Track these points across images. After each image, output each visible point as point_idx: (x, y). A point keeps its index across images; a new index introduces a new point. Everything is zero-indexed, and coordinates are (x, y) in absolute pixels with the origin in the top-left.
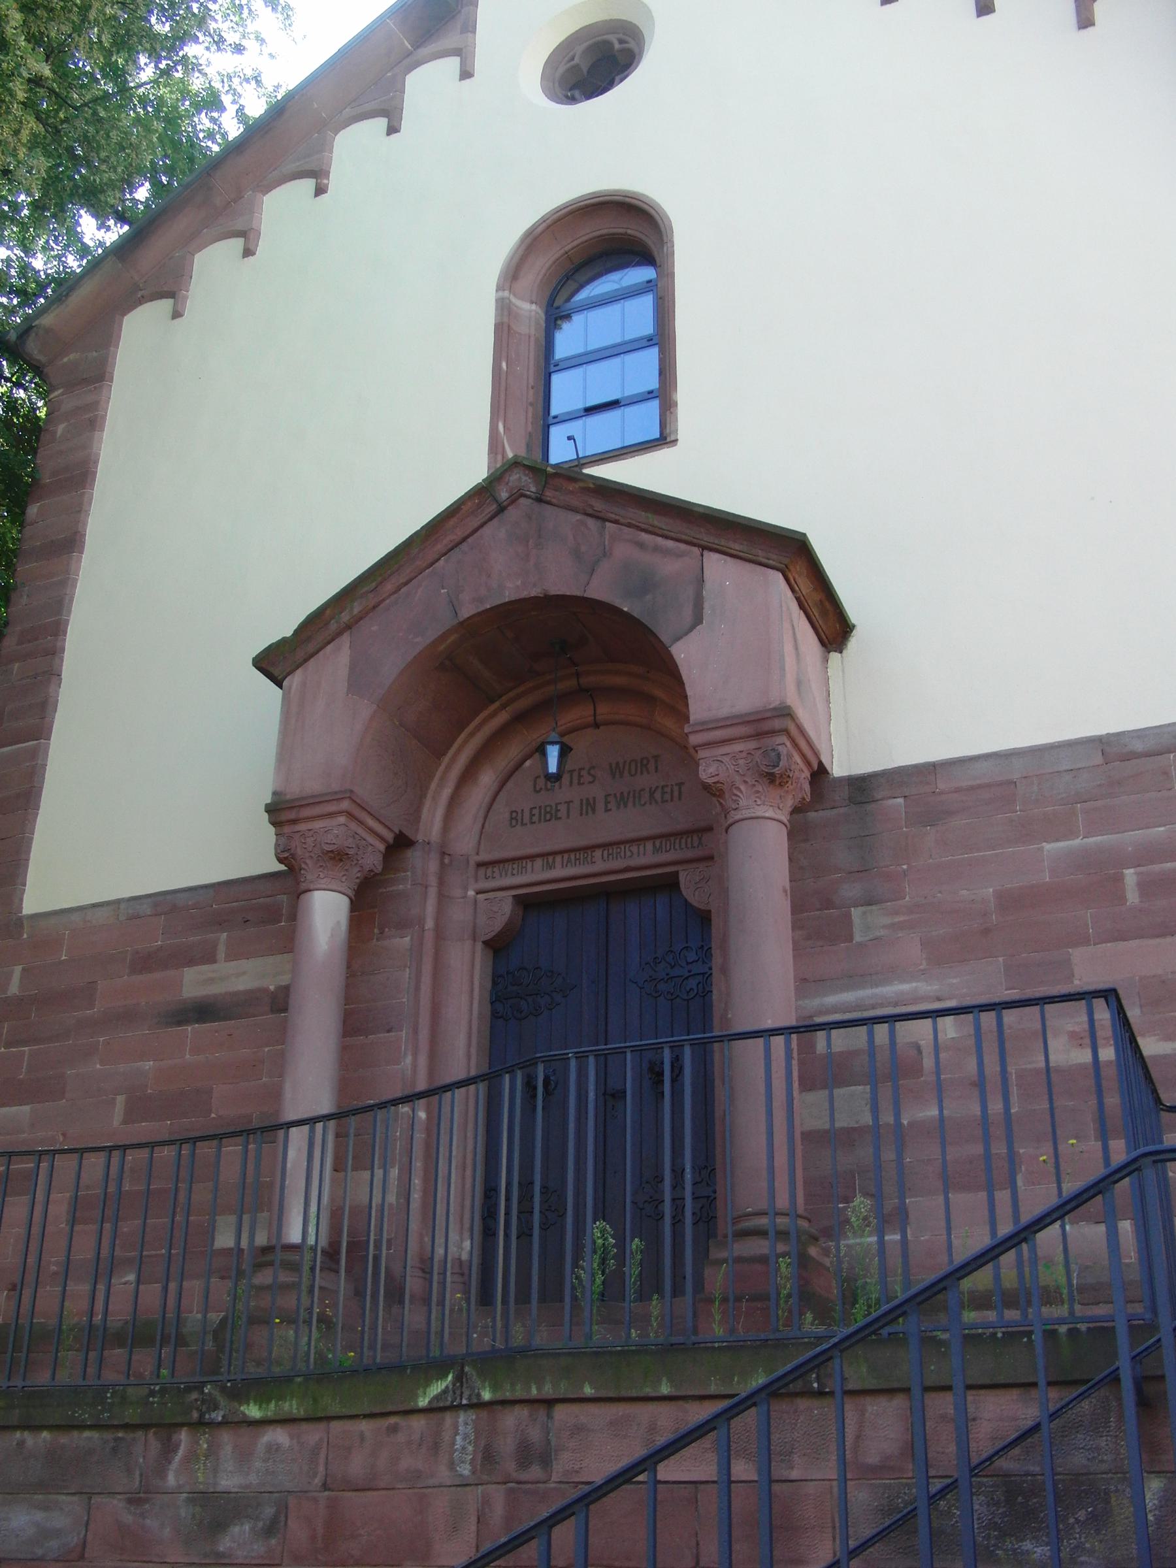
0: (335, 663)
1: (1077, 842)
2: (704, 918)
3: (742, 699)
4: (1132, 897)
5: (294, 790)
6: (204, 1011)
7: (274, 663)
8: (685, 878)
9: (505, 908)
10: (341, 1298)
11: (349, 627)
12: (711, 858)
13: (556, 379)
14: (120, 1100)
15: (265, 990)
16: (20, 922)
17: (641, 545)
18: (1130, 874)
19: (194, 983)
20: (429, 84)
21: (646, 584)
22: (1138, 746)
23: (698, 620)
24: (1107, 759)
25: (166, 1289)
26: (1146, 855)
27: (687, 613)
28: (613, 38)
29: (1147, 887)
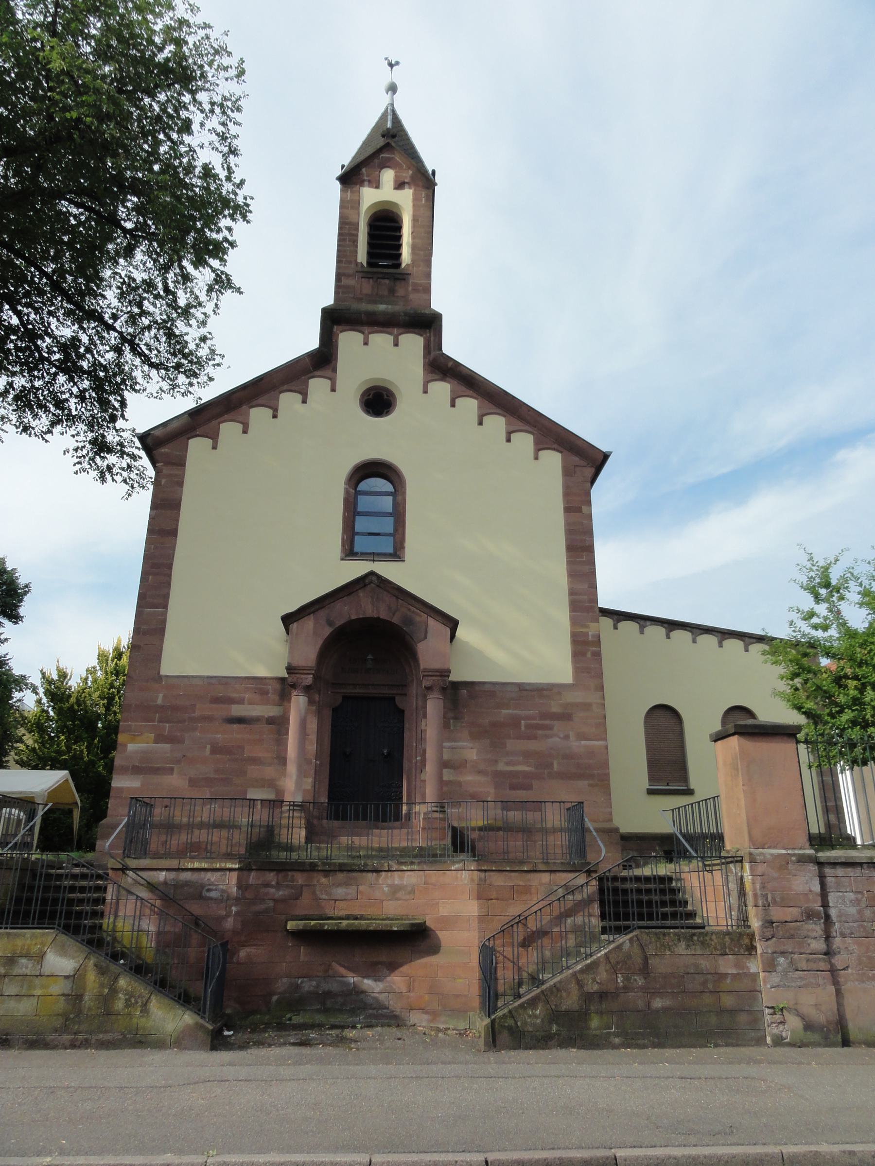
0: (309, 623)
1: (510, 711)
2: (403, 712)
3: (436, 665)
4: (523, 728)
5: (295, 663)
6: (240, 720)
7: (288, 620)
8: (397, 699)
9: (340, 700)
10: (600, 842)
11: (313, 612)
12: (405, 695)
13: (357, 518)
14: (208, 747)
15: (263, 716)
16: (159, 678)
17: (409, 609)
18: (523, 722)
19: (237, 710)
20: (317, 385)
21: (409, 621)
22: (528, 688)
23: (426, 637)
24: (520, 690)
25: (834, 864)
26: (527, 718)
27: (423, 637)
28: (384, 393)
29: (528, 726)
